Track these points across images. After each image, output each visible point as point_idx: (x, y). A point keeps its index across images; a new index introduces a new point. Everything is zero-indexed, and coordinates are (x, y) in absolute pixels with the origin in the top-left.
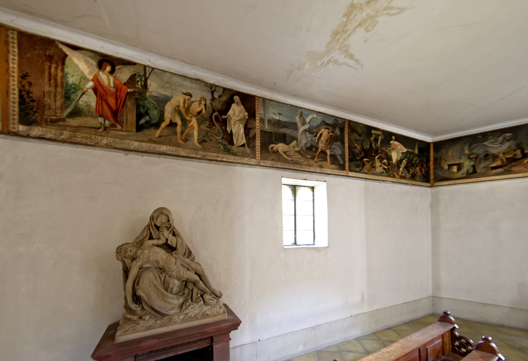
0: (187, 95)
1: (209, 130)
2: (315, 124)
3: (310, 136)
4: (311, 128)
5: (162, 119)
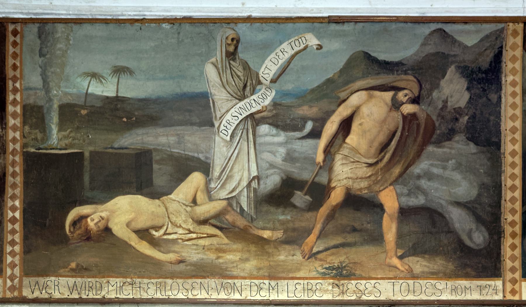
2: (313, 81)
3: (282, 137)
4: (287, 101)
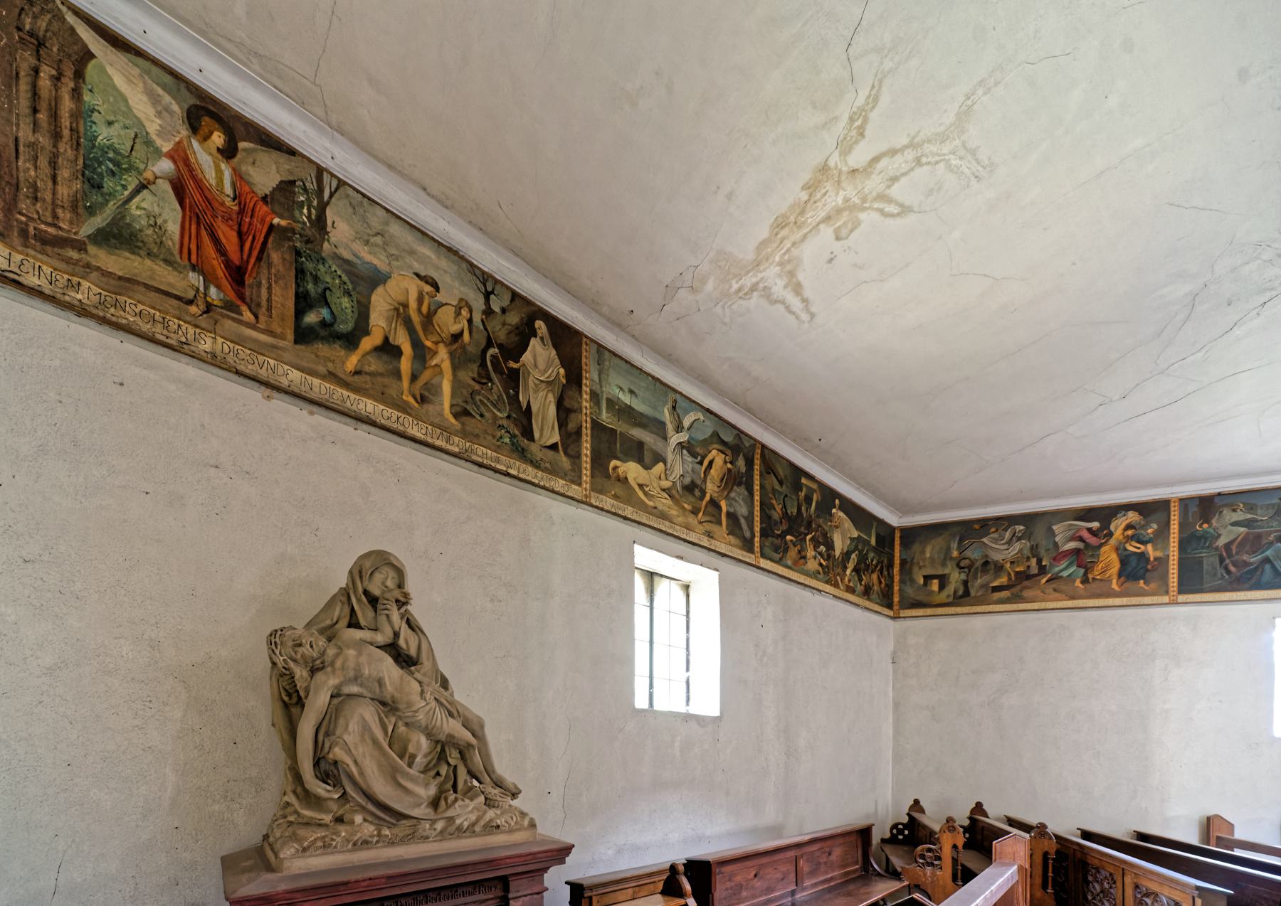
0: (427, 282)
1: (477, 387)
2: (701, 437)
5: (362, 328)
